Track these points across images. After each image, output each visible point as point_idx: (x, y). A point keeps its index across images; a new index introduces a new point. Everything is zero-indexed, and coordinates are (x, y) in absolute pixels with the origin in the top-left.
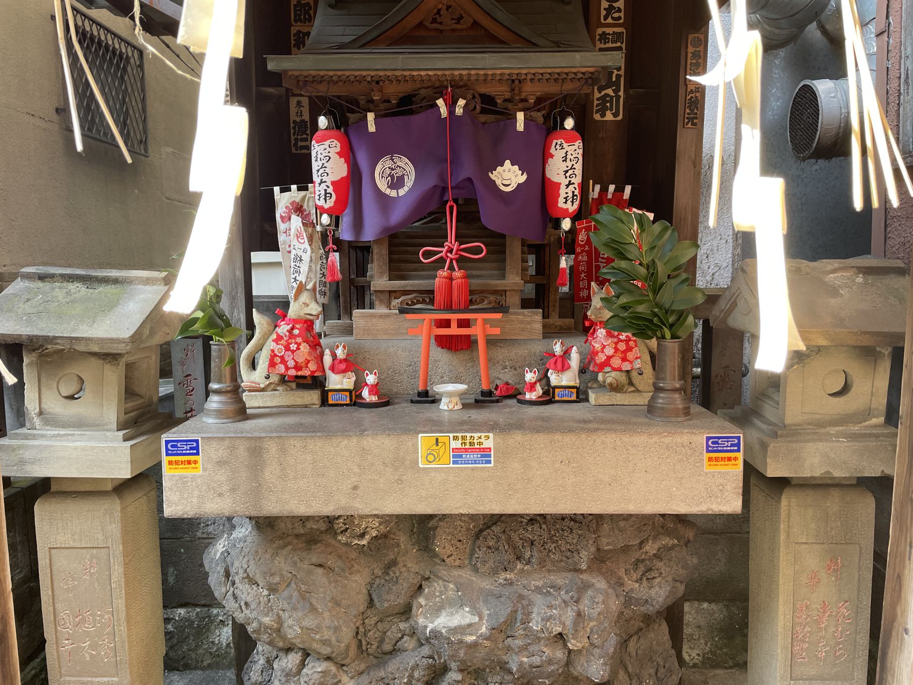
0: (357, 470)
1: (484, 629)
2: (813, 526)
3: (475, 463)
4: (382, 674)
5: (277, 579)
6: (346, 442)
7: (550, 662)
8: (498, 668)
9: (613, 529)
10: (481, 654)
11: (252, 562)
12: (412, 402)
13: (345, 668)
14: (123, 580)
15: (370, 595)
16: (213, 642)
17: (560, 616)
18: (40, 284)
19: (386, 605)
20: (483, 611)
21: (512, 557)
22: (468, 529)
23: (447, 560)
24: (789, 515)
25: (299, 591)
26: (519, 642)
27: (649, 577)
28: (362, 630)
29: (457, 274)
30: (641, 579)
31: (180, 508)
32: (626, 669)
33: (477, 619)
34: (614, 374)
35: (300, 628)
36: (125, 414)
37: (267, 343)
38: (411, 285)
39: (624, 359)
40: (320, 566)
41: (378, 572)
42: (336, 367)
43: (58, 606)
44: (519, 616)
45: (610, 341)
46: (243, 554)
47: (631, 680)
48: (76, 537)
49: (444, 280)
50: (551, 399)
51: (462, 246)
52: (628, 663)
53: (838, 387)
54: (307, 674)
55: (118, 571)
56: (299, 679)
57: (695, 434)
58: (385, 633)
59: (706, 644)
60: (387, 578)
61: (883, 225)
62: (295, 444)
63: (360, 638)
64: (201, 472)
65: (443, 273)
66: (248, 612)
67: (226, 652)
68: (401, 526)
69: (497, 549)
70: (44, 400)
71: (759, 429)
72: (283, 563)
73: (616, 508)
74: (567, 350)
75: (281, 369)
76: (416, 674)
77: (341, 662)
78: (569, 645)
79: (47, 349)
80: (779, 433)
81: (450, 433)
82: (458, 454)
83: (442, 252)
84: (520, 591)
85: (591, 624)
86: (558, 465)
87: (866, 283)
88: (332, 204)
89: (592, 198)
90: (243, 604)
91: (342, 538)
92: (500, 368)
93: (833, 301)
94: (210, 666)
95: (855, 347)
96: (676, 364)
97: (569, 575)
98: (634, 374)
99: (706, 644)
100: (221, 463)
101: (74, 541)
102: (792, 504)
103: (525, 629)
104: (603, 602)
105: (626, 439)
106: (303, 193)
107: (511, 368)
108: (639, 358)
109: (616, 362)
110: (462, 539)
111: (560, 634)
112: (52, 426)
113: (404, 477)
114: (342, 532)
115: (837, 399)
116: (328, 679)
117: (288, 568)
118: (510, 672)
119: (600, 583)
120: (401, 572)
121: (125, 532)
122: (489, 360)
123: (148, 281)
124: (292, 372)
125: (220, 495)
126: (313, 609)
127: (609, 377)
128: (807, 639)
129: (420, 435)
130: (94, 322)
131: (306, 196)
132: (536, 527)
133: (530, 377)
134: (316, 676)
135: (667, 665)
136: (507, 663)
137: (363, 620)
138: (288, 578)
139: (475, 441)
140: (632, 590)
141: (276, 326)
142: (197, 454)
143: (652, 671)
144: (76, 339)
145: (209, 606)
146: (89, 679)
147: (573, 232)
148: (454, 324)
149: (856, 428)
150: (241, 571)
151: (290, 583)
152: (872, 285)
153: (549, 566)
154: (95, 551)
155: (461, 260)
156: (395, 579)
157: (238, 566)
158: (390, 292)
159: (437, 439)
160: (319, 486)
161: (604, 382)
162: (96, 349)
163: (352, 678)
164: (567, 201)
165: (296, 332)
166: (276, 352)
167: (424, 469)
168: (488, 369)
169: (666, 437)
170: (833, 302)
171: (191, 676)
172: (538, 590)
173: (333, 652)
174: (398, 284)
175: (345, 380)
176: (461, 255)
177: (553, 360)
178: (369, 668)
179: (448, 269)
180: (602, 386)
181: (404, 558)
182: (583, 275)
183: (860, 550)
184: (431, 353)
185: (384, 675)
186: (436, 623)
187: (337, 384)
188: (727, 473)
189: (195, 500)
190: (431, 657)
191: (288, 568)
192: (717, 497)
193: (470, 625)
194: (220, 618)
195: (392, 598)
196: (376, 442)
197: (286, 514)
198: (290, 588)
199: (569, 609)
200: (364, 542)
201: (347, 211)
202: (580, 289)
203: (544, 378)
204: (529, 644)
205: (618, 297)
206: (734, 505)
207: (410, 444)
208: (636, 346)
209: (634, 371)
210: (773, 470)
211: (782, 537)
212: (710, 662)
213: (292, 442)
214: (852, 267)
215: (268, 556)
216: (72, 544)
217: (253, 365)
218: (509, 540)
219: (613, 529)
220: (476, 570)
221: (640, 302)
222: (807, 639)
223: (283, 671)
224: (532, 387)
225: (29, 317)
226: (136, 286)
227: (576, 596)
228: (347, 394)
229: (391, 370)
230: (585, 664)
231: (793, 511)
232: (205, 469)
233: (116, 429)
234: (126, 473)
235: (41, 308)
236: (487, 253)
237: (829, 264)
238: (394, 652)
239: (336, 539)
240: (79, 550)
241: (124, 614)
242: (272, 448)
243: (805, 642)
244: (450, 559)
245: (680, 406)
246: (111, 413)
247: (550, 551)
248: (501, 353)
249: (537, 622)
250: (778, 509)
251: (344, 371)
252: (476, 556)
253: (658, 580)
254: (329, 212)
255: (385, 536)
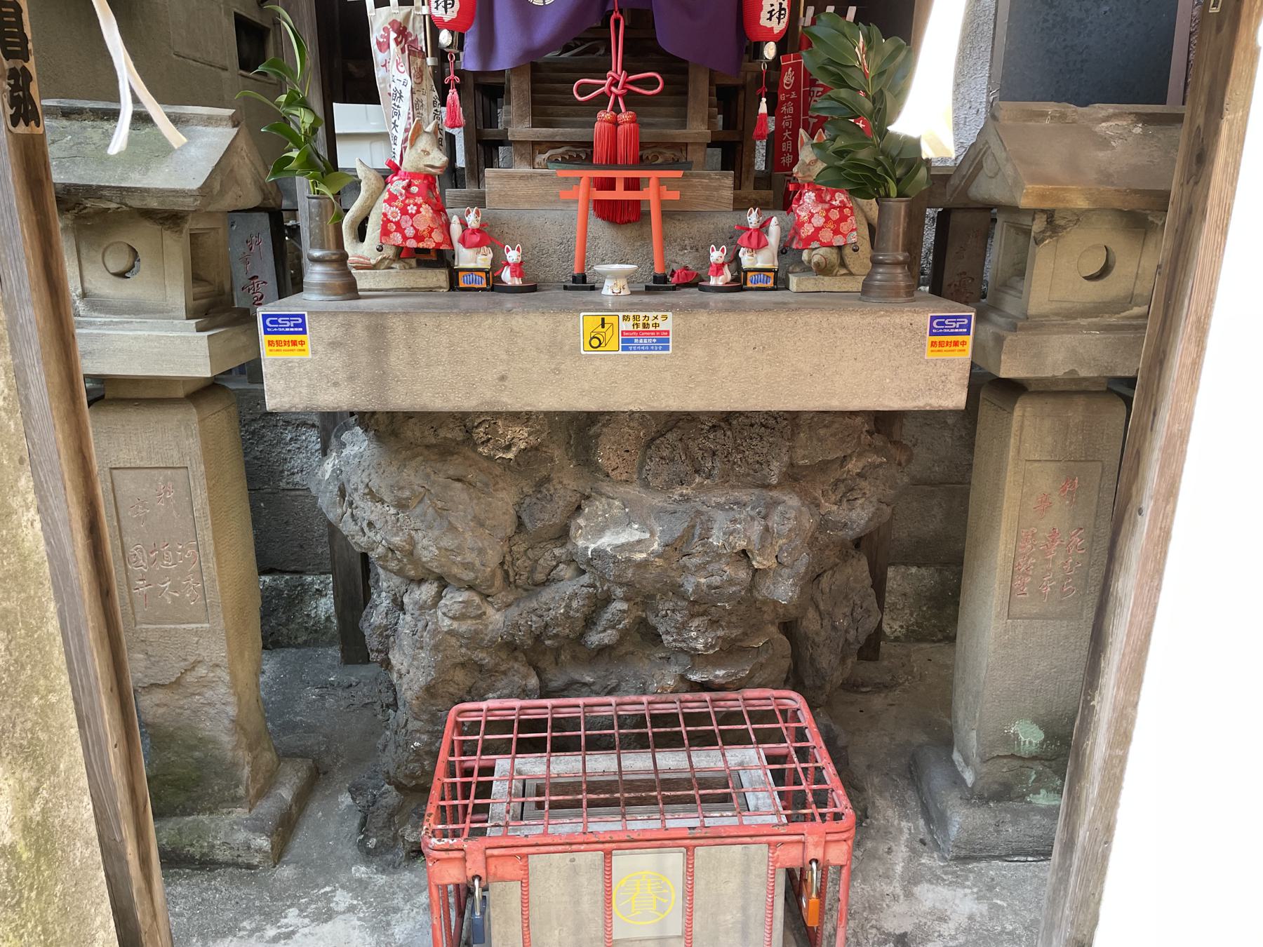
0: (505, 357)
1: (656, 546)
2: (1049, 440)
3: (650, 350)
4: (534, 604)
5: (407, 493)
6: (490, 321)
7: (731, 582)
8: (671, 594)
9: (811, 438)
10: (652, 574)
11: (374, 476)
12: (566, 288)
13: (489, 599)
14: (208, 507)
15: (519, 517)
16: (308, 615)
17: (745, 530)
18: (65, 122)
19: (539, 524)
20: (655, 527)
21: (687, 468)
22: (638, 437)
23: (612, 474)
24: (1022, 427)
25: (434, 508)
26: (696, 560)
27: (851, 497)
28: (508, 558)
29: (625, 116)
30: (841, 501)
31: (286, 399)
32: (817, 607)
33: (647, 535)
34: (823, 251)
35: (437, 548)
36: (194, 300)
37: (377, 205)
38: (562, 134)
39: (836, 232)
40: (459, 480)
41: (527, 490)
42: (467, 239)
43: (127, 539)
44: (698, 531)
45: (819, 208)
46: (362, 468)
47: (822, 619)
48: (144, 454)
49: (607, 124)
50: (741, 286)
51: (631, 77)
52: (819, 600)
53: (1095, 268)
54: (446, 605)
55: (201, 497)
56: (435, 612)
57: (918, 313)
58: (536, 561)
59: (911, 615)
60: (539, 496)
61: (1182, 84)
62: (426, 323)
63: (506, 568)
64: (310, 356)
65: (605, 115)
66: (372, 534)
67: (326, 627)
68: (555, 438)
69: (672, 460)
70: (87, 277)
71: (996, 325)
72: (413, 476)
73: (817, 404)
74: (765, 222)
75: (397, 238)
76: (575, 604)
77: (486, 592)
78: (754, 563)
79: (86, 208)
80: (1020, 324)
81: (618, 311)
82: (627, 341)
83: (603, 85)
84: (699, 508)
85: (781, 542)
86: (750, 352)
87: (1144, 135)
88: (455, 15)
89: (803, 27)
90: (365, 525)
91: (484, 450)
92: (678, 248)
93: (1101, 154)
94: (306, 644)
95: (1120, 212)
96: (901, 230)
97: (757, 491)
98: (848, 251)
99: (911, 615)
100: (334, 345)
101: (142, 459)
102: (1027, 414)
103: (703, 545)
104: (796, 518)
105: (834, 319)
106: (406, 9)
107: (691, 248)
108: (855, 230)
109: (826, 235)
110: (629, 448)
111: (744, 551)
112: (100, 311)
113: (563, 366)
114: (483, 443)
115: (1093, 283)
116: (470, 610)
117: (420, 482)
118: (683, 597)
119: (793, 501)
120: (555, 489)
121: (206, 451)
122: (665, 238)
123: (209, 121)
124: (412, 244)
125: (336, 384)
126: (452, 528)
127: (816, 255)
128: (1031, 573)
129: (582, 314)
130: (147, 169)
131: (410, 12)
132: (719, 433)
133: (716, 256)
134: (456, 606)
135: (865, 606)
136: (682, 586)
137: (510, 547)
138: (420, 493)
139: (650, 322)
140: (829, 513)
141: (386, 184)
142: (304, 332)
143: (847, 610)
144: (128, 189)
145: (301, 572)
146: (173, 626)
147: (775, 64)
148: (620, 185)
149: (1113, 320)
150: (361, 486)
151: (422, 499)
152: (1153, 136)
153: (733, 481)
154: (169, 472)
155: (632, 100)
156: (548, 497)
157: (356, 480)
158: (534, 143)
159: (603, 319)
160: (458, 375)
161: (810, 261)
162: (154, 204)
163: (498, 610)
164: (771, 16)
165: (414, 189)
166: (390, 217)
167: (587, 356)
168: (663, 248)
169: (882, 316)
170: (1102, 155)
171: (282, 654)
172: (719, 506)
173: (476, 578)
174: (544, 133)
175: (480, 257)
176: (629, 90)
177: (746, 235)
178: (517, 600)
179: (612, 110)
180: (807, 269)
181: (559, 475)
182: (786, 134)
183: (1103, 469)
184: (589, 227)
185: (537, 606)
186: (599, 543)
187: (470, 262)
188: (952, 361)
189: (304, 391)
190: (593, 586)
191: (420, 482)
192: (937, 390)
193: (639, 541)
194: (317, 587)
195: (547, 518)
196: (528, 322)
197: (418, 409)
198: (422, 505)
199: (756, 523)
200: (510, 455)
201: (472, 28)
202: (782, 154)
203: (735, 260)
204: (708, 562)
205: (834, 140)
206: (956, 398)
207: (570, 325)
208: (852, 214)
209: (848, 247)
210: (1009, 370)
211: (1012, 453)
212: (915, 635)
213: (423, 319)
214: (1131, 113)
215: (394, 469)
216: (139, 463)
217: (361, 234)
218: (686, 449)
219: (811, 438)
220: (646, 485)
221: (863, 146)
222: (1031, 573)
223: (416, 603)
224: (719, 269)
225: (60, 162)
226: (194, 127)
227: (764, 512)
228: (483, 275)
229: (537, 249)
230: (772, 587)
231: (1027, 423)
232: (314, 352)
233: (185, 317)
234: (204, 371)
235: (74, 152)
236: (665, 83)
237: (1102, 109)
238: (547, 582)
239: (475, 451)
240: (149, 471)
241: (212, 548)
242: (397, 326)
243: (1028, 575)
244: (616, 472)
245: (902, 284)
246: (177, 295)
247: (735, 463)
248: (680, 229)
249: (718, 537)
250: (1011, 413)
251: (478, 245)
252: (647, 468)
253: (860, 502)
254: (450, 25)
255: (536, 449)
